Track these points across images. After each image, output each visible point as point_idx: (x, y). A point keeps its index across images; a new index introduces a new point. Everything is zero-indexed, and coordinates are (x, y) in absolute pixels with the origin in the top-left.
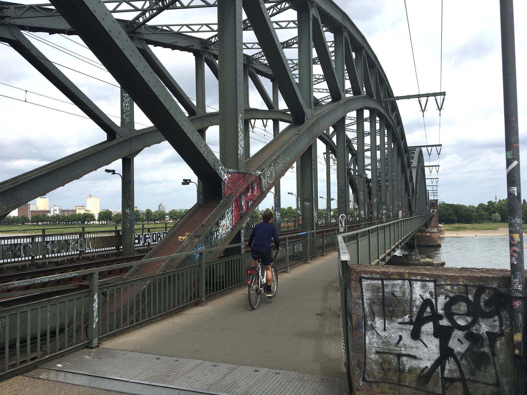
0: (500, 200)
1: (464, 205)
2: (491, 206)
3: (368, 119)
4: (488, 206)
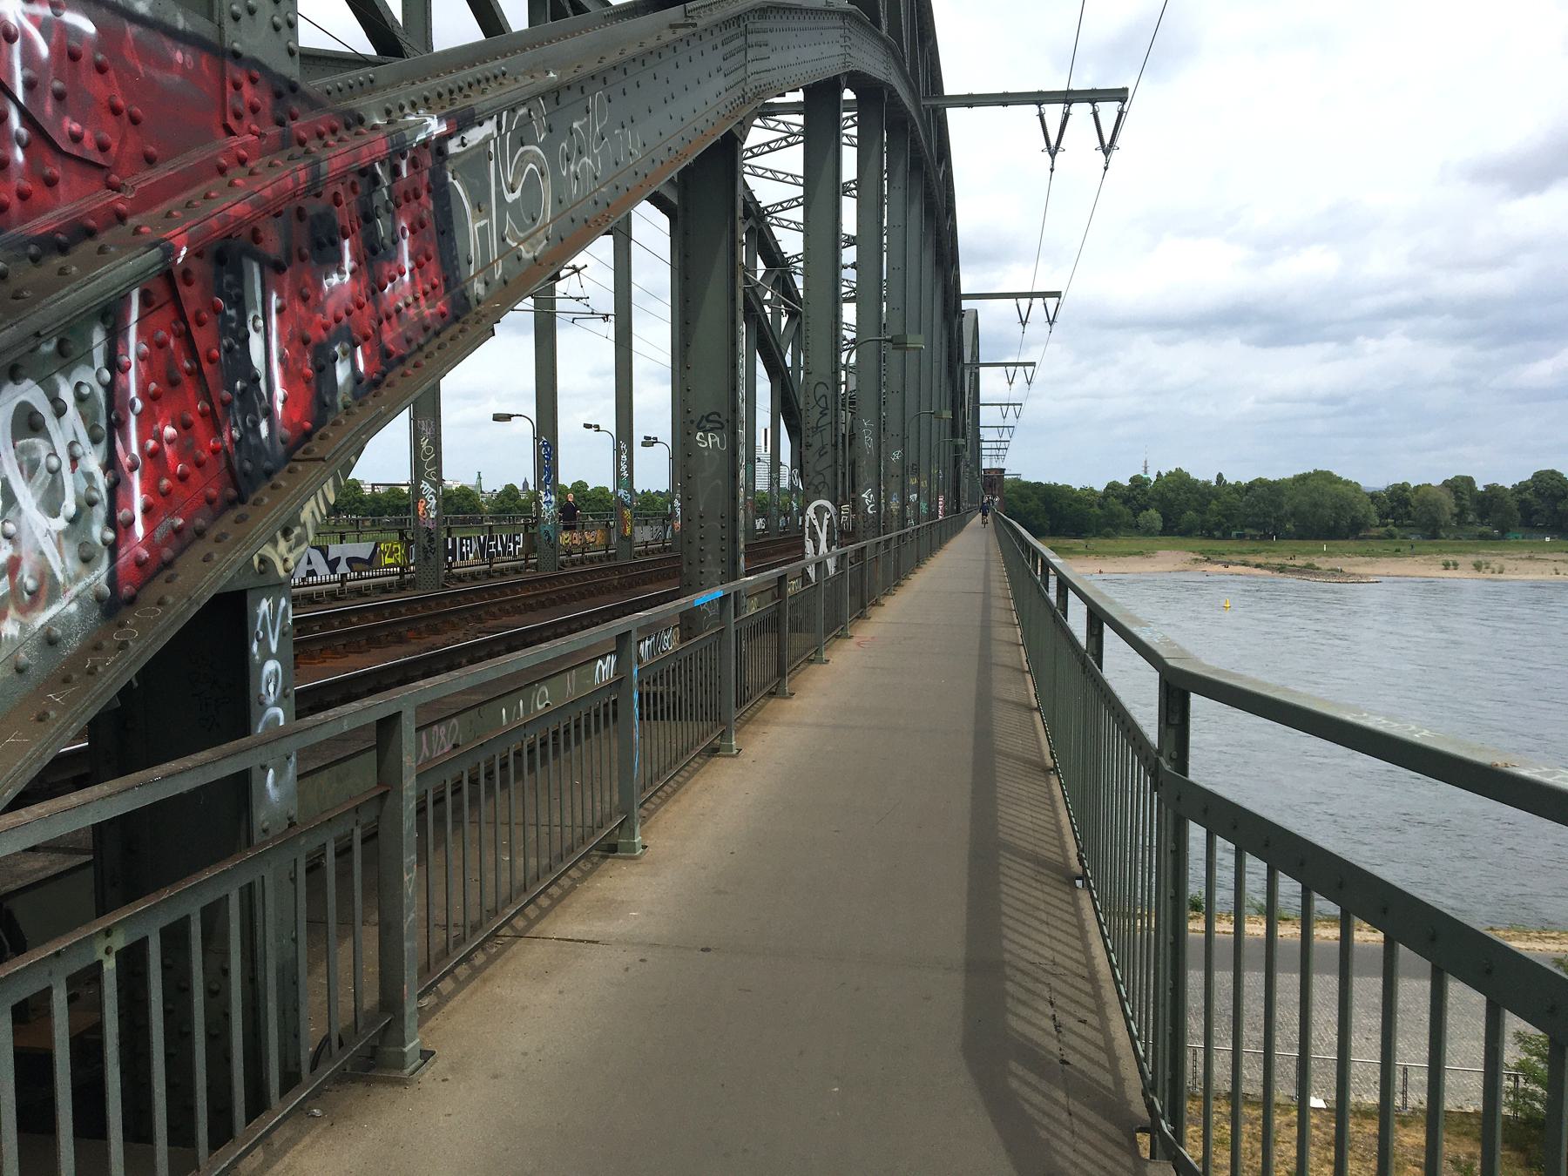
0: (1159, 474)
1: (1069, 487)
2: (1138, 490)
3: (853, 186)
4: (1130, 489)
